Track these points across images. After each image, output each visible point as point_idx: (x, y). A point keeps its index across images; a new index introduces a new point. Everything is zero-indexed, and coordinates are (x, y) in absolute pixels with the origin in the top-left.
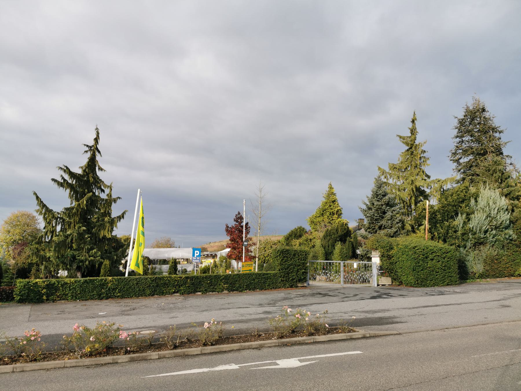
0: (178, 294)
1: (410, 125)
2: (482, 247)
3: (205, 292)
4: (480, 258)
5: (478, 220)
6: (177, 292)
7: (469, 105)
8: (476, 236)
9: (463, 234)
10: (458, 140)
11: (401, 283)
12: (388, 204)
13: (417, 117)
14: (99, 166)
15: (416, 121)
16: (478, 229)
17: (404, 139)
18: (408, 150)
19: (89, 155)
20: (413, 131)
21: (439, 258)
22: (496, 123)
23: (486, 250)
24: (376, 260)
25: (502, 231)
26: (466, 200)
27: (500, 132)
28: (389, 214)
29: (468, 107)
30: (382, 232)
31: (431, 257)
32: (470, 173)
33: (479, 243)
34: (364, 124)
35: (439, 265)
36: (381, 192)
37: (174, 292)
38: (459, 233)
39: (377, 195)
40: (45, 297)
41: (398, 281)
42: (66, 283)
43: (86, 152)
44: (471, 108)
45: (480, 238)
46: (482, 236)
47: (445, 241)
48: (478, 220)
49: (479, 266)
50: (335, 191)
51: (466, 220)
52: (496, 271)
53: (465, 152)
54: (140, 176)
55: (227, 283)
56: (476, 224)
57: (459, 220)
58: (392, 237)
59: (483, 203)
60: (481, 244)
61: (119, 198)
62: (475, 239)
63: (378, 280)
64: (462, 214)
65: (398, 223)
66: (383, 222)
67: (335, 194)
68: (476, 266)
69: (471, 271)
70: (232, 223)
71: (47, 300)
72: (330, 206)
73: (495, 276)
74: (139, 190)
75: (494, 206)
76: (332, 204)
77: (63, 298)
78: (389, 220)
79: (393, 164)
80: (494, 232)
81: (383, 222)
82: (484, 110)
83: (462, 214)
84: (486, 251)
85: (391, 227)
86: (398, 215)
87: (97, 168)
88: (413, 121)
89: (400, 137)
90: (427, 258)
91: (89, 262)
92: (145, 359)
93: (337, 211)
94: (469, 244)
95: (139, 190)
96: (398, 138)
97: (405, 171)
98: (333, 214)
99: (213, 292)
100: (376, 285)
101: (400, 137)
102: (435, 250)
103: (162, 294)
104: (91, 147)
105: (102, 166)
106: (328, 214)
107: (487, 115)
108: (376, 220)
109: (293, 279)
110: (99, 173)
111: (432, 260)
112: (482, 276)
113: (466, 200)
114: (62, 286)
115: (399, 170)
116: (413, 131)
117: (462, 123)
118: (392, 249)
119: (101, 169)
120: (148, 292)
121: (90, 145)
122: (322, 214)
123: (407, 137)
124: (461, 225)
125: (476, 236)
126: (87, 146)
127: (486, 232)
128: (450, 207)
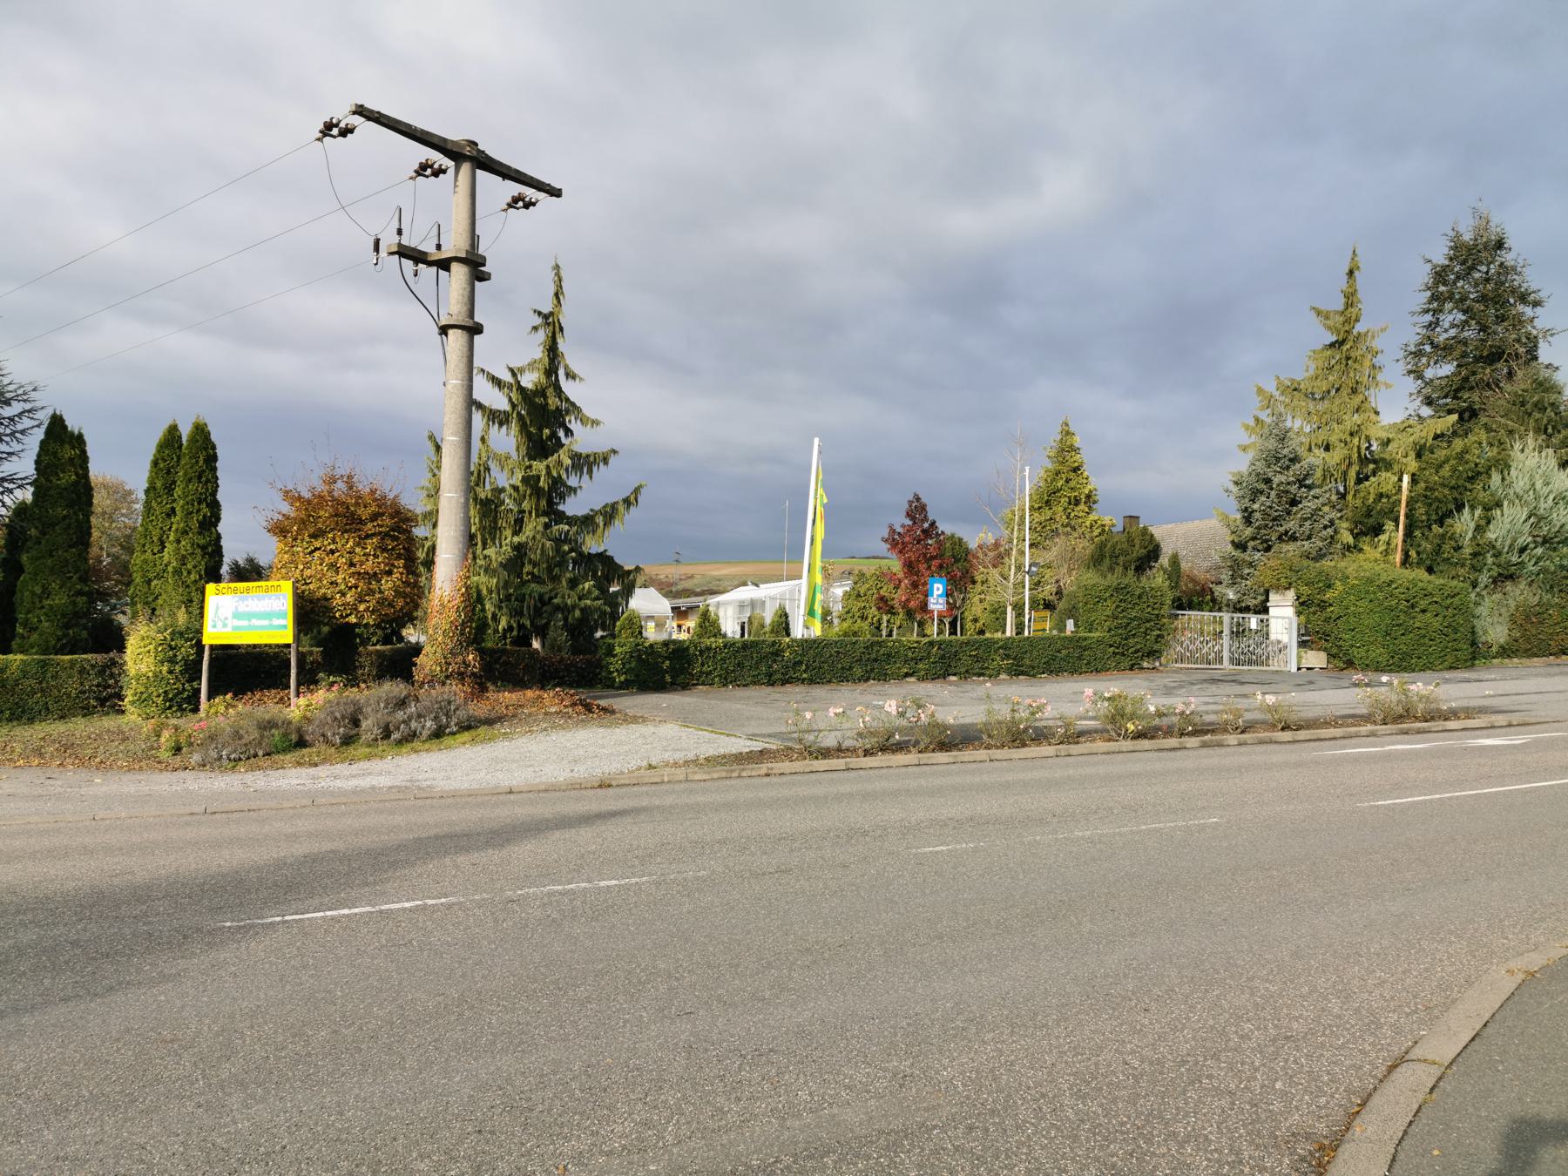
0: (912, 679)
1: (1342, 282)
2: (1509, 586)
3: (966, 675)
4: (1503, 610)
5: (1509, 524)
6: (911, 675)
7: (1462, 229)
8: (1502, 559)
9: (1475, 555)
10: (1428, 317)
11: (1350, 664)
12: (1301, 483)
13: (1362, 260)
14: (566, 367)
15: (1356, 273)
16: (1508, 542)
17: (1327, 318)
18: (1332, 345)
19: (541, 335)
20: (1350, 298)
21: (1440, 610)
22: (1531, 279)
23: (1518, 592)
24: (1283, 618)
25: (1555, 550)
26: (1479, 473)
27: (1536, 304)
28: (1308, 506)
29: (1458, 235)
30: (1290, 548)
31: (1423, 604)
32: (1460, 402)
33: (1506, 576)
34: (967, 225)
35: (1436, 623)
36: (1285, 451)
37: (907, 675)
38: (1467, 551)
39: (1278, 459)
40: (668, 678)
41: (1344, 662)
42: (709, 649)
43: (535, 328)
44: (1467, 237)
45: (1509, 564)
46: (1515, 559)
47: (1430, 570)
48: (1509, 524)
49: (1499, 628)
50: (1077, 441)
51: (1483, 523)
52: (1535, 641)
53: (1443, 351)
54: (278, 370)
55: (1008, 657)
56: (1504, 532)
57: (1465, 523)
58: (1315, 559)
59: (1521, 483)
60: (1511, 577)
61: (615, 452)
62: (1499, 566)
63: (1299, 658)
64: (1473, 508)
65: (1325, 527)
66: (1291, 525)
67: (1076, 450)
68: (1496, 632)
69: (1483, 639)
70: (900, 521)
71: (672, 684)
72: (1067, 481)
73: (1530, 653)
74: (816, 441)
75: (1546, 490)
76: (1072, 475)
77: (705, 679)
78: (1306, 519)
79: (1293, 381)
80: (1539, 551)
81: (1291, 525)
82: (1500, 245)
83: (1473, 508)
84: (1520, 594)
85: (1309, 538)
86: (1326, 509)
87: (561, 372)
88: (1351, 273)
89: (1319, 313)
90: (1413, 606)
91: (582, 610)
92: (1220, 745)
93: (1088, 497)
94: (1484, 579)
95: (816, 441)
96: (1313, 314)
97: (1323, 398)
98: (1077, 502)
99: (980, 675)
100: (1294, 669)
101: (1319, 313)
102: (1430, 588)
103: (883, 677)
104: (546, 317)
105: (574, 368)
106: (1064, 500)
107: (1508, 258)
108: (1274, 519)
109: (1137, 651)
110: (567, 387)
111: (1424, 611)
112: (1506, 652)
113: (1479, 473)
114: (701, 652)
115: (1311, 396)
116: (1350, 298)
117: (1440, 275)
118: (1329, 586)
119: (570, 375)
120: (858, 671)
121: (546, 311)
122: (1047, 502)
123: (1336, 312)
124: (1470, 535)
125: (1502, 559)
126: (540, 313)
127: (1522, 550)
128: (1446, 491)
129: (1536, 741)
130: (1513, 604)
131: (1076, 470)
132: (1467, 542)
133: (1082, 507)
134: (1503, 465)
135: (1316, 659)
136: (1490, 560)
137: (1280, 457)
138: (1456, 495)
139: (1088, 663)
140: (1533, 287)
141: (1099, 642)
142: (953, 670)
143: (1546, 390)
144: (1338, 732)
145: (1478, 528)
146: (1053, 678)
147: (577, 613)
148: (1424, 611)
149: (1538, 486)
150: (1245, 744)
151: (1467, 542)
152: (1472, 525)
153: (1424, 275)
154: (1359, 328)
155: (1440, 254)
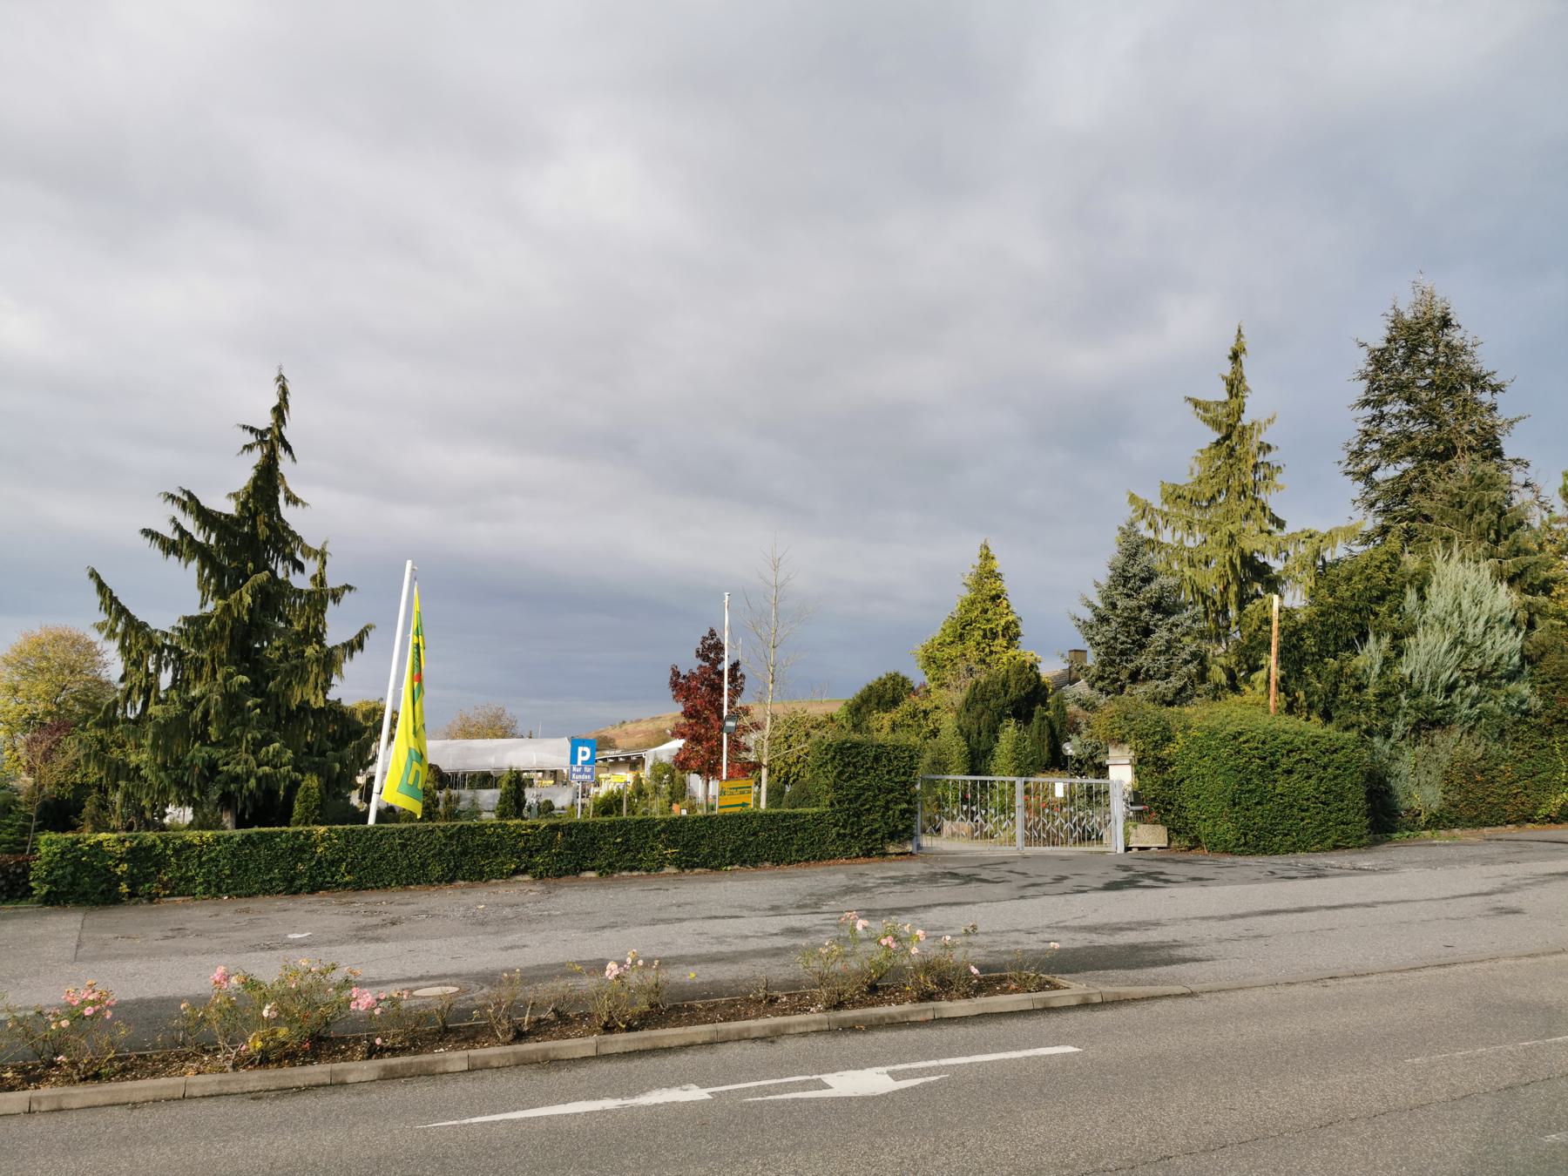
0: (527, 878)
1: (1227, 368)
2: (1438, 735)
3: (608, 870)
4: (1432, 767)
5: (1427, 653)
6: (524, 872)
7: (1402, 307)
9: (1383, 696)
10: (1369, 411)
11: (1196, 843)
13: (1248, 342)
14: (287, 490)
15: (1242, 357)
16: (1427, 681)
17: (1206, 410)
18: (1218, 443)
19: (257, 456)
20: (1235, 386)
22: (1484, 360)
23: (1451, 743)
25: (1498, 686)
27: (1495, 389)
28: (1160, 637)
29: (1398, 314)
30: (1140, 690)
31: (1285, 763)
33: (1430, 723)
34: (1088, 364)
35: (1309, 788)
36: (1136, 569)
37: (516, 872)
39: (1127, 580)
40: (124, 888)
41: (1187, 836)
42: (190, 846)
43: (249, 447)
44: (1408, 316)
45: (1431, 707)
46: (1439, 701)
47: (1327, 716)
48: (1427, 653)
49: (1428, 790)
50: (998, 565)
53: (1390, 450)
54: (413, 522)
55: (675, 843)
56: (1420, 666)
57: (1371, 654)
58: (1170, 704)
59: (1441, 603)
60: (1436, 724)
61: (350, 588)
62: (1418, 709)
63: (1127, 834)
64: (1378, 636)
65: (1186, 662)
66: (1143, 660)
67: (998, 576)
68: (1421, 792)
69: (1406, 805)
70: (690, 664)
71: (132, 895)
72: (985, 611)
73: (1476, 822)
74: (409, 563)
75: (1475, 611)
76: (989, 605)
78: (1160, 653)
79: (1175, 487)
80: (1474, 689)
81: (1143, 660)
82: (1446, 322)
83: (1378, 636)
84: (1451, 745)
85: (1168, 675)
86: (1187, 640)
87: (281, 496)
89: (1197, 404)
90: (1272, 766)
91: (259, 780)
92: (429, 1073)
93: (1007, 628)
94: (1399, 727)
95: (409, 563)
96: (1190, 406)
98: (995, 635)
99: (632, 869)
100: (1121, 850)
101: (1197, 404)
102: (1297, 742)
104: (262, 434)
105: (297, 491)
106: (978, 635)
107: (1455, 336)
108: (1122, 653)
110: (287, 512)
111: (1289, 772)
112: (1437, 822)
114: (177, 852)
116: (1235, 386)
117: (1380, 360)
118: (1169, 739)
119: (293, 500)
120: (436, 870)
121: (262, 427)
122: (961, 635)
123: (1218, 404)
124: (1377, 669)
125: (1421, 701)
126: (252, 430)
127: (1450, 689)
129: (956, 1082)
130: (1446, 760)
131: (995, 598)
132: (1373, 680)
133: (1001, 641)
134: (1422, 583)
135: (1152, 836)
136: (1405, 703)
137: (1131, 575)
138: (1358, 620)
139: (800, 850)
140: (1486, 369)
141: (818, 819)
142: (588, 863)
143: (1488, 487)
144: (700, 1031)
145: (1386, 661)
146: (714, 875)
147: (253, 782)
148: (1289, 772)
149: (1465, 606)
150: (486, 1066)
151: (1373, 680)
152: (1379, 659)
153: (1362, 361)
154: (1246, 420)
155: (1377, 337)
